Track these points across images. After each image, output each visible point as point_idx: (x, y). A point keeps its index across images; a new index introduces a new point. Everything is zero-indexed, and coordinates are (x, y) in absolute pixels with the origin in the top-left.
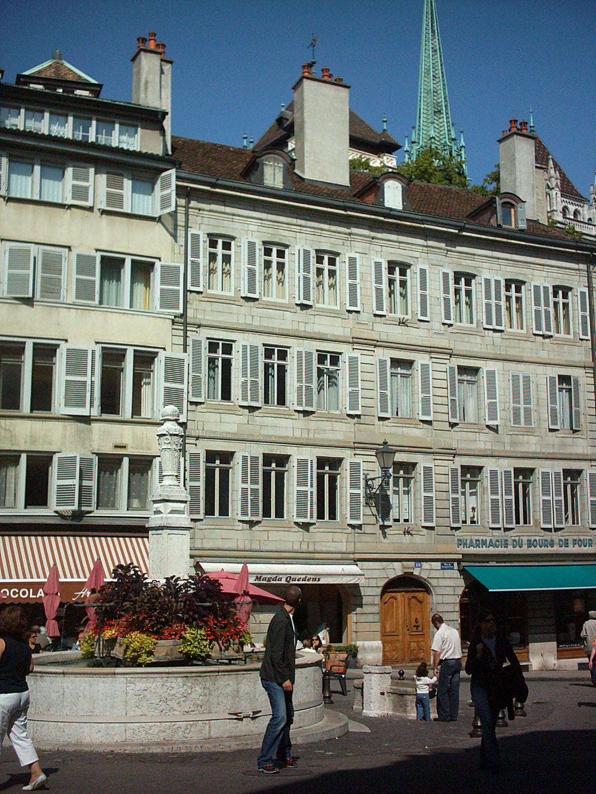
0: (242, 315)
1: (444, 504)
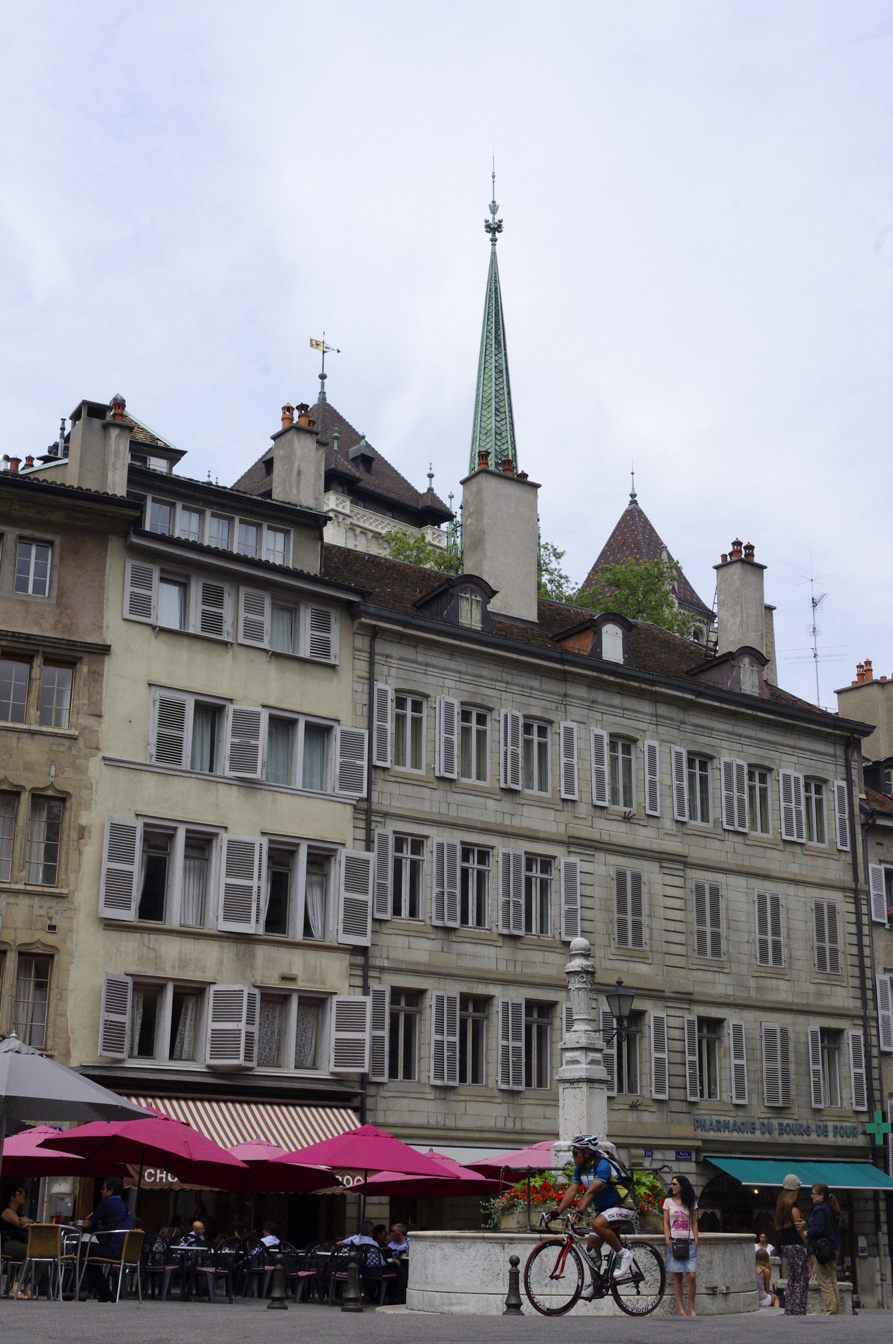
0: (432, 802)
1: (678, 1070)
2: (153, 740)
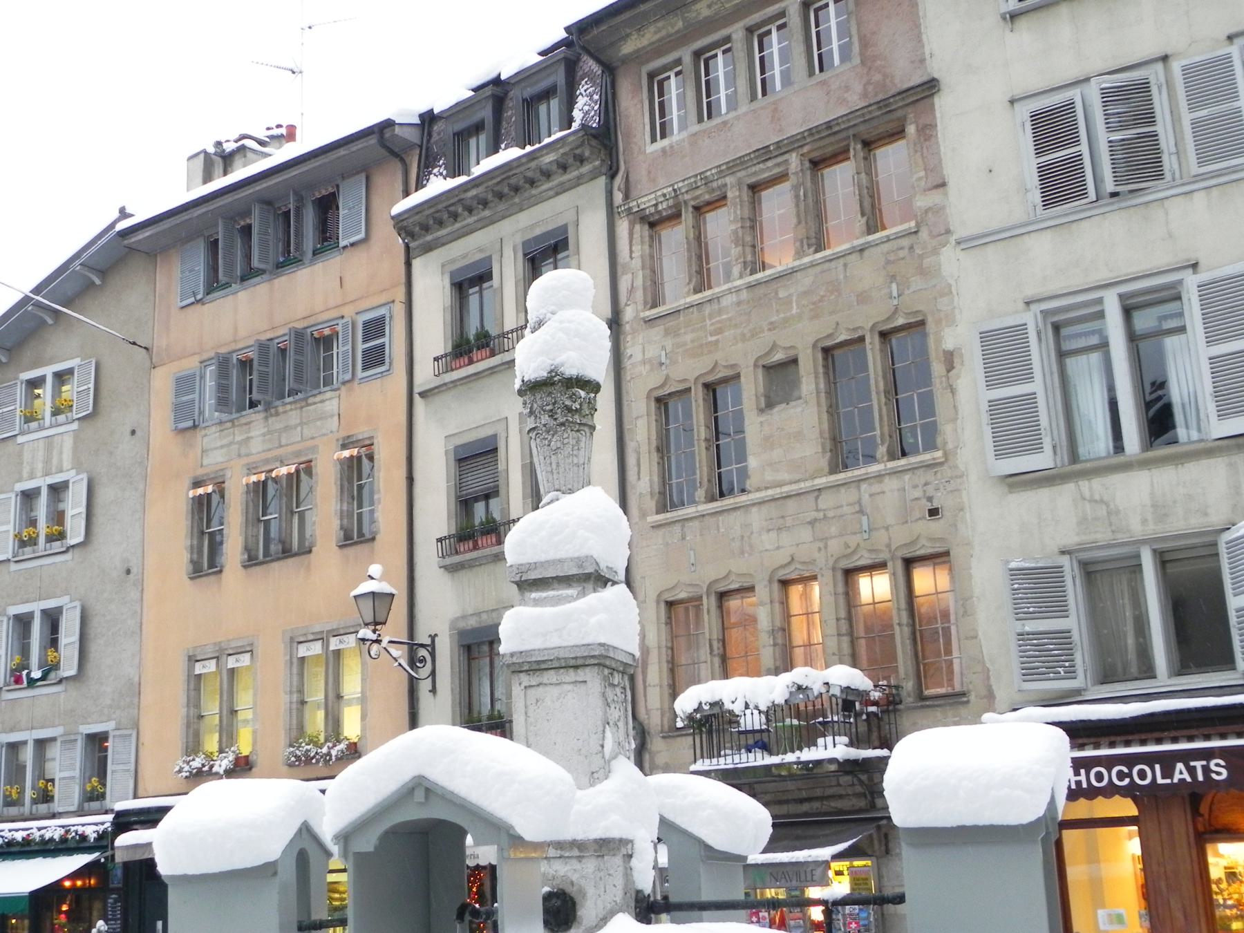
2: (1033, 180)
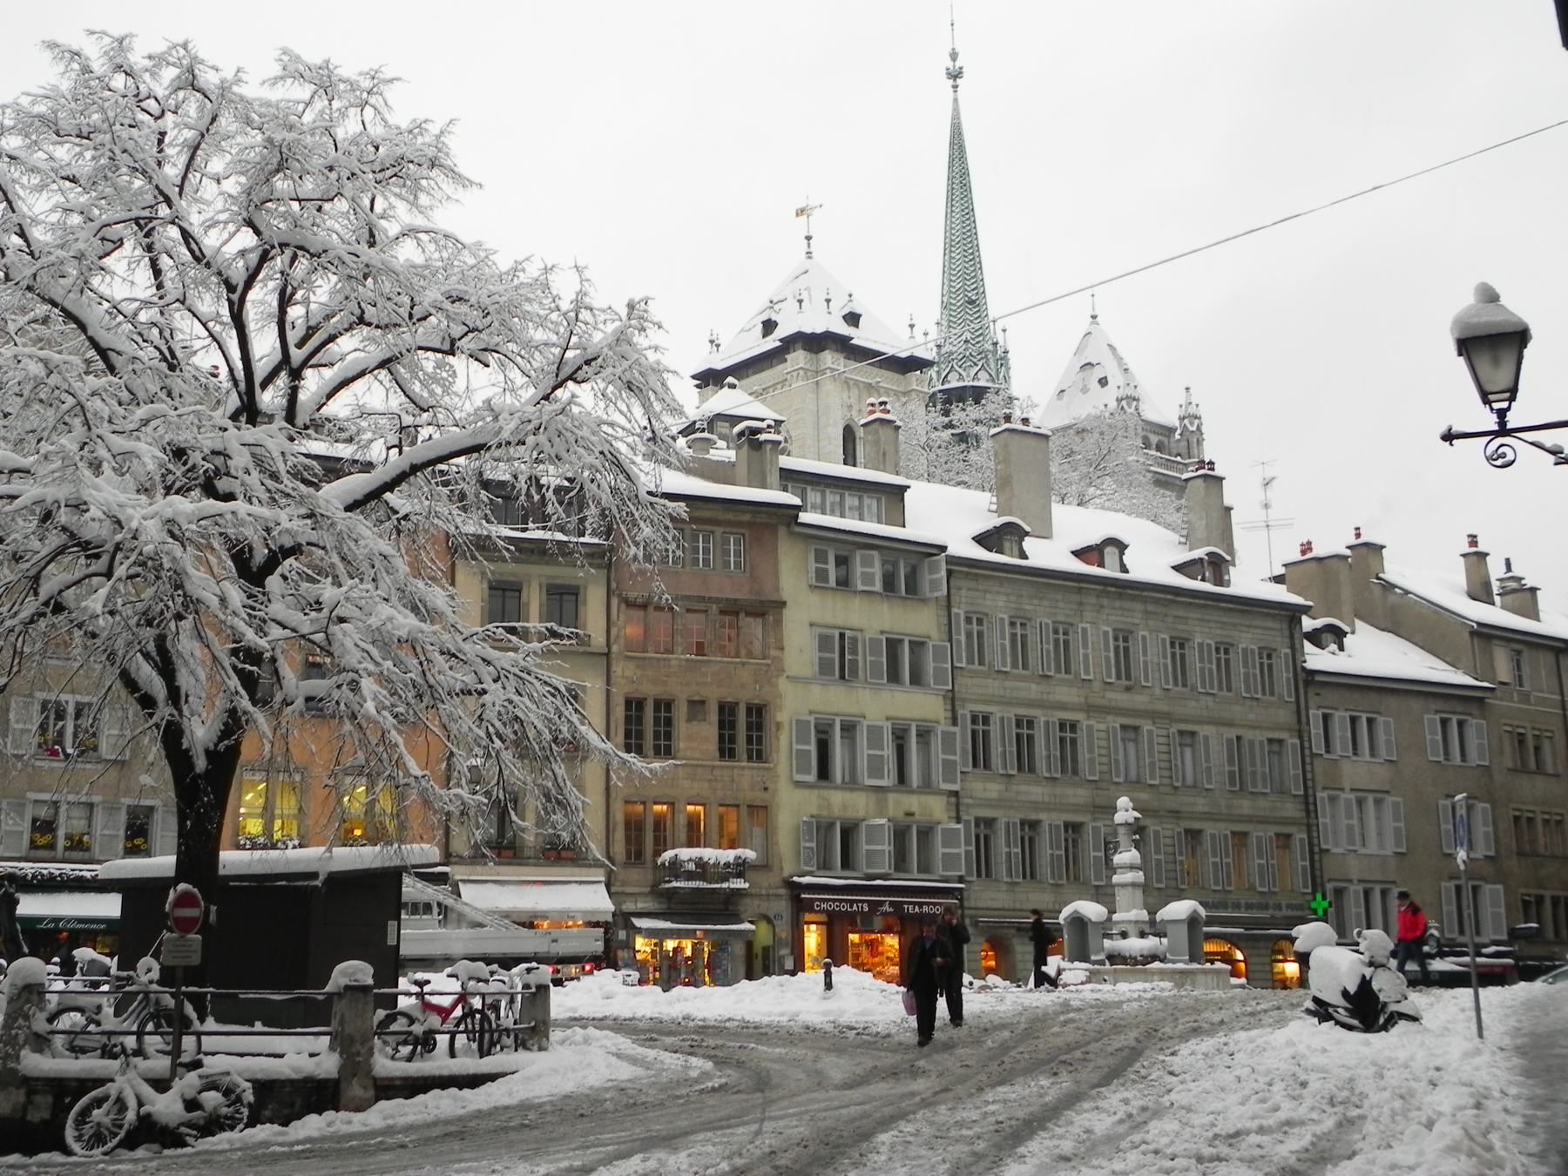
0: (993, 686)
2: (816, 661)
